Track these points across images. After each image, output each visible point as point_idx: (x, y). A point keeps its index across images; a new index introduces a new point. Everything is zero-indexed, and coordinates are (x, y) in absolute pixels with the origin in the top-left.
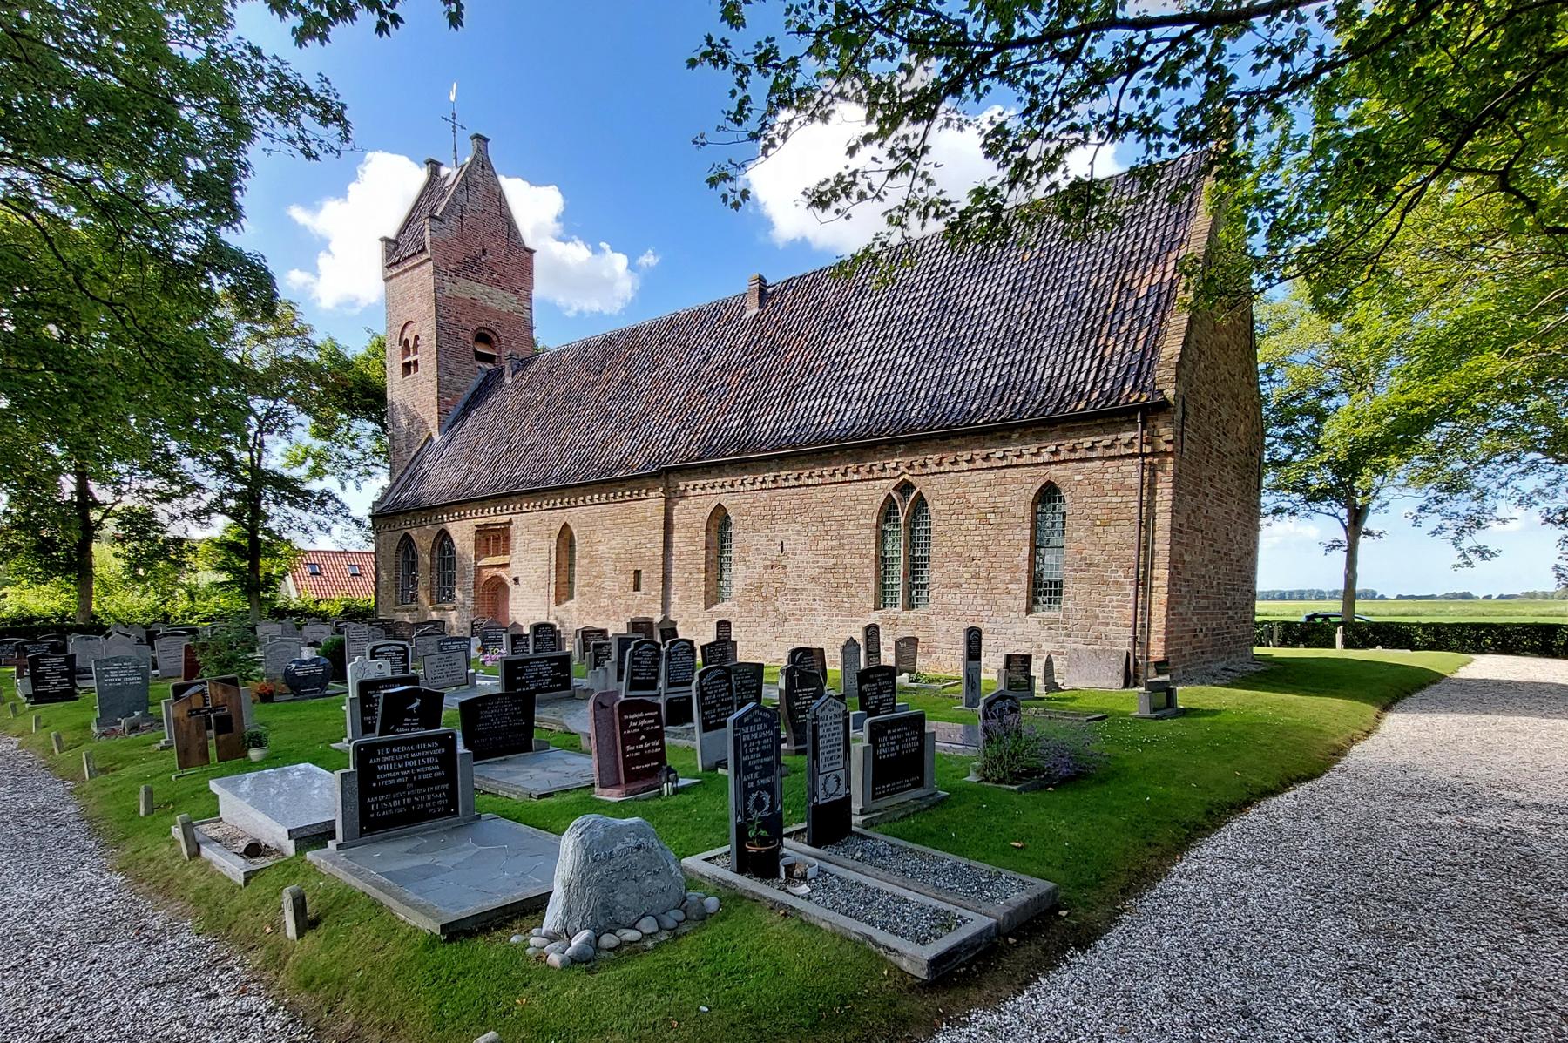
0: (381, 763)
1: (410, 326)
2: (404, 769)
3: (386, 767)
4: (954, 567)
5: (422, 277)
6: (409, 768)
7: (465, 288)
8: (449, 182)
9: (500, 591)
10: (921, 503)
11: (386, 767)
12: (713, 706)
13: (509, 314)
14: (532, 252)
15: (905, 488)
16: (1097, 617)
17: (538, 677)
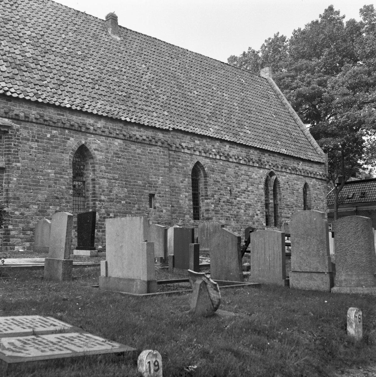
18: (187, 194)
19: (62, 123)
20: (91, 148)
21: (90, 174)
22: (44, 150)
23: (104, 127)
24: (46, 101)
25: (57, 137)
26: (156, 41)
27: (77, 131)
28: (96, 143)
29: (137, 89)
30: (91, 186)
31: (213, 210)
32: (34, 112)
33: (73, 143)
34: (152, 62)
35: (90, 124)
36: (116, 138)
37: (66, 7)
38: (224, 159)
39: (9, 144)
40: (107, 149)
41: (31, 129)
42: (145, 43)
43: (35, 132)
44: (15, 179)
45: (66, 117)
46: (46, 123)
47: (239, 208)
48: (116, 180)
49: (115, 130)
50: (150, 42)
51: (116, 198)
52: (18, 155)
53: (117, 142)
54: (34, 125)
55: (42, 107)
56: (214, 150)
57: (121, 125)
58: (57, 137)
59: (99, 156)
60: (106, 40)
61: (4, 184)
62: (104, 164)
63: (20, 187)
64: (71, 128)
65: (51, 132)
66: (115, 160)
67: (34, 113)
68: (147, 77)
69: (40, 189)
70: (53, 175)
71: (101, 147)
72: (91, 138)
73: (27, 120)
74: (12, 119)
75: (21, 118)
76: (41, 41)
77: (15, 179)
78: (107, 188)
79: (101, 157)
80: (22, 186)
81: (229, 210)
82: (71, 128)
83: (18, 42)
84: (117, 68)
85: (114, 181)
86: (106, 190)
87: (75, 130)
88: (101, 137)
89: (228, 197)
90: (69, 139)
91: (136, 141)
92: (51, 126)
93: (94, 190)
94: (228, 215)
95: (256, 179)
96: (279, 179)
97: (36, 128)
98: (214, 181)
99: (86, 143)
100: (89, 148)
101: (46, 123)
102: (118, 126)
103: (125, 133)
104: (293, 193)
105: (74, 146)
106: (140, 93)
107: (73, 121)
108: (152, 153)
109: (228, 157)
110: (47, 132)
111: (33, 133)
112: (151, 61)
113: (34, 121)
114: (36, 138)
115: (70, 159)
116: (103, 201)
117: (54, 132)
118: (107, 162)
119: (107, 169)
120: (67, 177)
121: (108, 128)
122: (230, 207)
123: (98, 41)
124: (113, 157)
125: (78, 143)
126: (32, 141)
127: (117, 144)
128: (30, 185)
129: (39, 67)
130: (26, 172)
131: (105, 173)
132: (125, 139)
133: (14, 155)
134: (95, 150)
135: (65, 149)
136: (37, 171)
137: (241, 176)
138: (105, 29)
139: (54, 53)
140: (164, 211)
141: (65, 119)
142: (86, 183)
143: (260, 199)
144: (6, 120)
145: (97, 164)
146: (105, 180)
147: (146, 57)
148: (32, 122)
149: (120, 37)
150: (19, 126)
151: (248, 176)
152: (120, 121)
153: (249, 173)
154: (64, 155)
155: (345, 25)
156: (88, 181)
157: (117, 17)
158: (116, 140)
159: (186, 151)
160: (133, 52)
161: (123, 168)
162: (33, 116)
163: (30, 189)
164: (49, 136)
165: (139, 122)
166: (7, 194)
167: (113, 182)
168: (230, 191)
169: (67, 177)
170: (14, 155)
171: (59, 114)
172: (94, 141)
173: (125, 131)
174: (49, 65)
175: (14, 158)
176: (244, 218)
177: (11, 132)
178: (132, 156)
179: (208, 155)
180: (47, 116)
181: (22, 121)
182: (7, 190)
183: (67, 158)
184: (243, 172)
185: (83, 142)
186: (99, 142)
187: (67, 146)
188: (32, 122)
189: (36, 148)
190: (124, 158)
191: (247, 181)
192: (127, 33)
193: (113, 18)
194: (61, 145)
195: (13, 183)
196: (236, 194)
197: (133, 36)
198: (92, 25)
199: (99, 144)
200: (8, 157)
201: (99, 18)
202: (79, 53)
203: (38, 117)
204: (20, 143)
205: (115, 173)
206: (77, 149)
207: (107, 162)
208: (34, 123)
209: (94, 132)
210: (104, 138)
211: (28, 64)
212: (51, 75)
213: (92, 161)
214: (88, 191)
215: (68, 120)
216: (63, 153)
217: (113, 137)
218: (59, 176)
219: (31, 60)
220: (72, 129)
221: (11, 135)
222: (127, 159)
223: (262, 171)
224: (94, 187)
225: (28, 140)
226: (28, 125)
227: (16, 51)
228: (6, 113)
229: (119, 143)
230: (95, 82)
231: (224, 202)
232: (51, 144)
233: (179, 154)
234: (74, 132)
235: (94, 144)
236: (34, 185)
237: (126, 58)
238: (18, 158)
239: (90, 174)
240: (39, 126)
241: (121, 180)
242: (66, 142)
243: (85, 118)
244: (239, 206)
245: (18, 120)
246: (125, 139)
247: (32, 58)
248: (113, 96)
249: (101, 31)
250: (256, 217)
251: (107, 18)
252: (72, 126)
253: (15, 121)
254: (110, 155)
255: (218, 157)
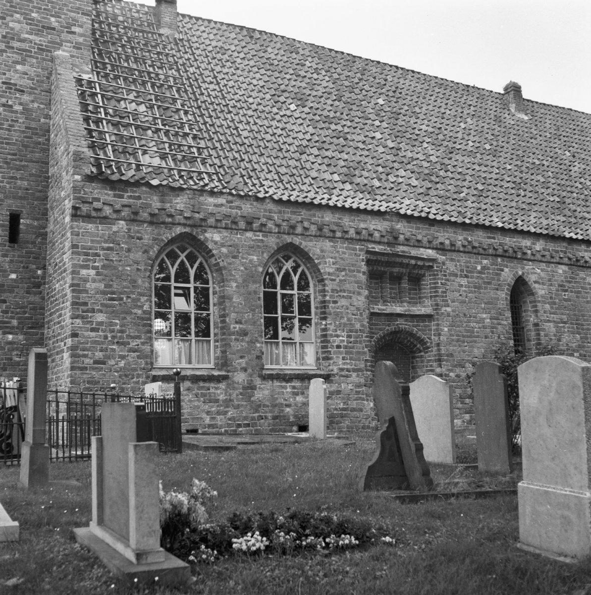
19: (494, 249)
20: (529, 281)
21: (531, 316)
22: (475, 287)
23: (544, 250)
24: (475, 221)
25: (488, 269)
26: (572, 113)
27: (512, 258)
28: (536, 273)
29: (569, 189)
30: (533, 333)
32: (460, 238)
33: (508, 275)
34: (576, 146)
35: (526, 247)
36: (559, 263)
37: (452, 82)
39: (435, 283)
40: (550, 280)
41: (459, 261)
42: (559, 118)
43: (463, 264)
44: (446, 329)
45: (498, 240)
46: (475, 251)
48: (565, 323)
49: (557, 252)
50: (565, 116)
51: (568, 349)
52: (446, 296)
53: (561, 269)
54: (461, 254)
55: (468, 230)
57: (565, 244)
58: (488, 269)
59: (541, 291)
60: (513, 122)
61: (433, 337)
62: (547, 301)
63: (453, 340)
64: (505, 255)
65: (481, 263)
66: (561, 295)
67: (460, 238)
68: (576, 168)
69: (475, 342)
70: (488, 320)
71: (542, 278)
72: (529, 266)
73: (453, 249)
74: (436, 249)
75: (446, 248)
76: (441, 137)
77: (446, 329)
78: (555, 335)
79: (543, 292)
80: (455, 337)
82: (505, 255)
83: (417, 143)
84: (537, 162)
85: (562, 325)
86: (553, 338)
87: (509, 257)
88: (541, 264)
90: (502, 270)
92: (481, 254)
93: (539, 339)
97: (464, 258)
99: (523, 274)
100: (527, 280)
101: (475, 251)
102: (561, 246)
103: (571, 256)
105: (509, 279)
106: (575, 195)
107: (506, 244)
110: (476, 263)
111: (460, 265)
112: (574, 144)
113: (462, 249)
114: (465, 273)
115: (506, 298)
117: (485, 262)
118: (551, 298)
119: (552, 308)
120: (505, 323)
121: (549, 251)
123: (503, 125)
124: (557, 290)
125: (514, 275)
126: (461, 276)
128: (464, 336)
129: (449, 174)
130: (458, 319)
131: (550, 314)
132: (571, 265)
133: (443, 296)
134: (535, 282)
135: (499, 285)
136: (470, 317)
138: (505, 107)
139: (460, 151)
141: (496, 243)
142: (525, 330)
144: (430, 251)
145: (539, 302)
146: (552, 325)
147: (565, 139)
148: (459, 251)
149: (526, 114)
150: (444, 257)
152: (564, 239)
154: (499, 292)
156: (528, 327)
157: (520, 87)
158: (560, 266)
160: (549, 136)
161: (572, 305)
162: (460, 242)
163: (464, 342)
164: (479, 268)
165: (522, 228)
166: (439, 350)
167: (561, 327)
169: (505, 323)
170: (443, 296)
171: (489, 238)
172: (532, 271)
173: (570, 252)
174: (460, 170)
175: (443, 301)
177: (437, 267)
178: (582, 288)
180: (475, 241)
181: (447, 250)
182: (438, 345)
183: (503, 296)
185: (520, 273)
186: (539, 271)
187: (502, 279)
188: (459, 251)
189: (466, 285)
190: (572, 292)
192: (533, 107)
193: (514, 89)
194: (493, 279)
195: (445, 335)
197: (543, 111)
198: (489, 102)
199: (539, 274)
200: (435, 301)
201: (494, 91)
202: (488, 147)
203: (466, 244)
204: (448, 280)
205: (562, 314)
206: (513, 282)
207: (551, 298)
208: (461, 252)
209: (532, 258)
210: (544, 264)
211: (436, 172)
212: (466, 184)
213: (532, 298)
214: (529, 340)
215: (501, 244)
216: (497, 289)
217: (556, 263)
218: (495, 321)
219: (439, 167)
220: (505, 257)
221: (437, 271)
222: (575, 292)
224: (539, 335)
225: (456, 275)
226: (454, 255)
227: (418, 156)
228: (430, 242)
229: (563, 271)
230: (517, 186)
232: (482, 278)
234: (508, 259)
235: (534, 273)
236: (468, 337)
237: (485, 127)
238: (447, 301)
239: (531, 316)
240: (467, 255)
241: (572, 324)
242: (499, 275)
243: (520, 240)
245: (443, 250)
246: (571, 265)
247: (439, 163)
248: (544, 203)
249: (501, 110)
251: (506, 89)
252: (506, 251)
253: (440, 252)
254: (554, 288)
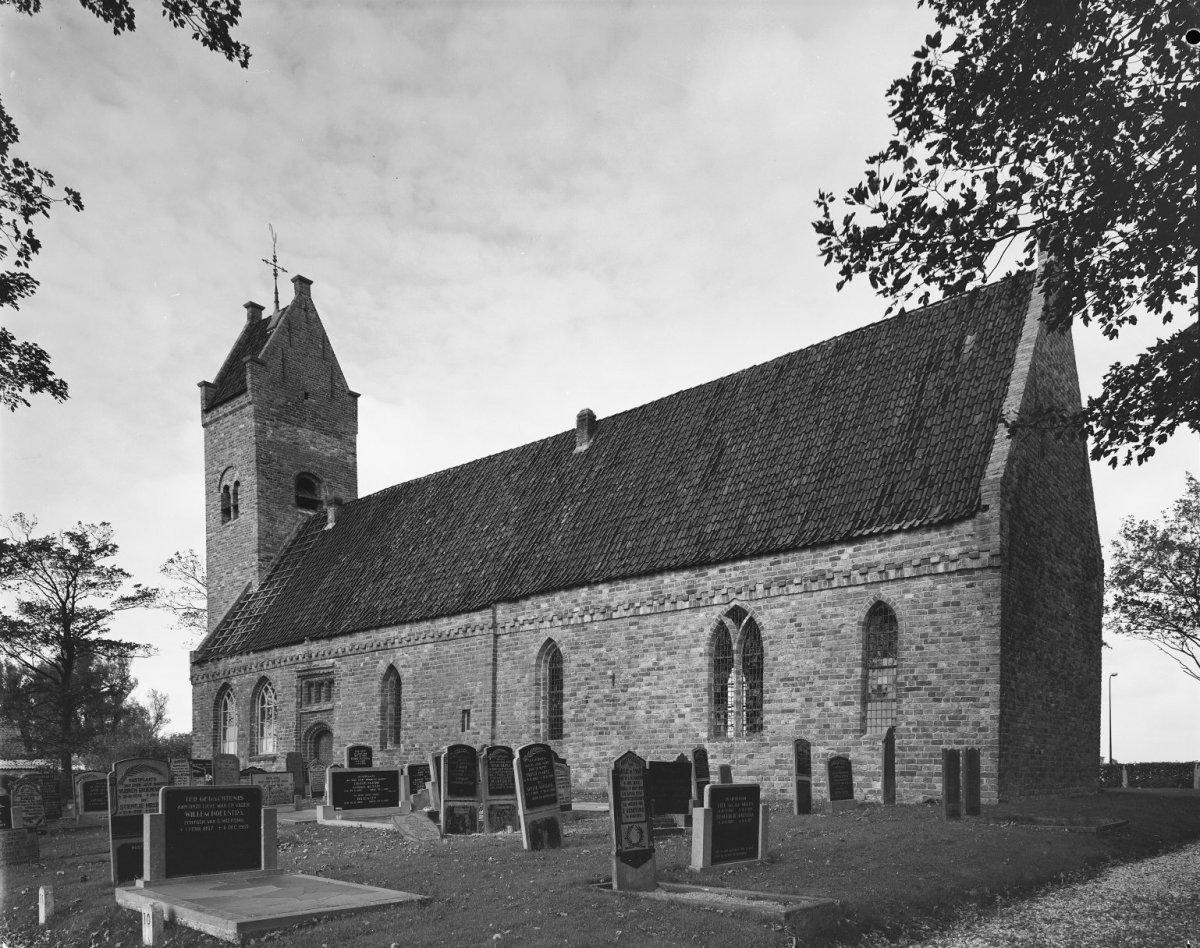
0: (189, 810)
1: (229, 472)
2: (210, 818)
3: (193, 814)
4: (782, 693)
5: (242, 419)
6: (215, 818)
7: (285, 433)
8: (272, 324)
9: (324, 740)
10: (753, 631)
11: (193, 814)
12: (535, 783)
13: (331, 459)
14: (356, 396)
15: (736, 613)
16: (930, 736)
17: (366, 791)
18: (526, 699)
31: (572, 720)
33: (382, 666)
38: (601, 617)
47: (631, 709)
56: (577, 609)
81: (608, 714)
89: (607, 691)
91: (449, 639)
94: (602, 724)
95: (685, 637)
96: (759, 619)
98: (579, 666)
104: (816, 644)
108: (469, 649)
109: (607, 611)
116: (409, 729)
117: (367, 659)
122: (611, 709)
127: (426, 651)
137: (642, 642)
140: (482, 732)
143: (693, 681)
151: (662, 635)
153: (666, 630)
155: (862, 234)
159: (527, 627)
164: (362, 665)
168: (613, 677)
176: (646, 726)
179: (566, 620)
184: (650, 631)
191: (658, 647)
196: (627, 681)
223: (702, 615)
231: (596, 701)
233: (518, 636)
244: (633, 704)
250: (678, 721)
255: (587, 618)
